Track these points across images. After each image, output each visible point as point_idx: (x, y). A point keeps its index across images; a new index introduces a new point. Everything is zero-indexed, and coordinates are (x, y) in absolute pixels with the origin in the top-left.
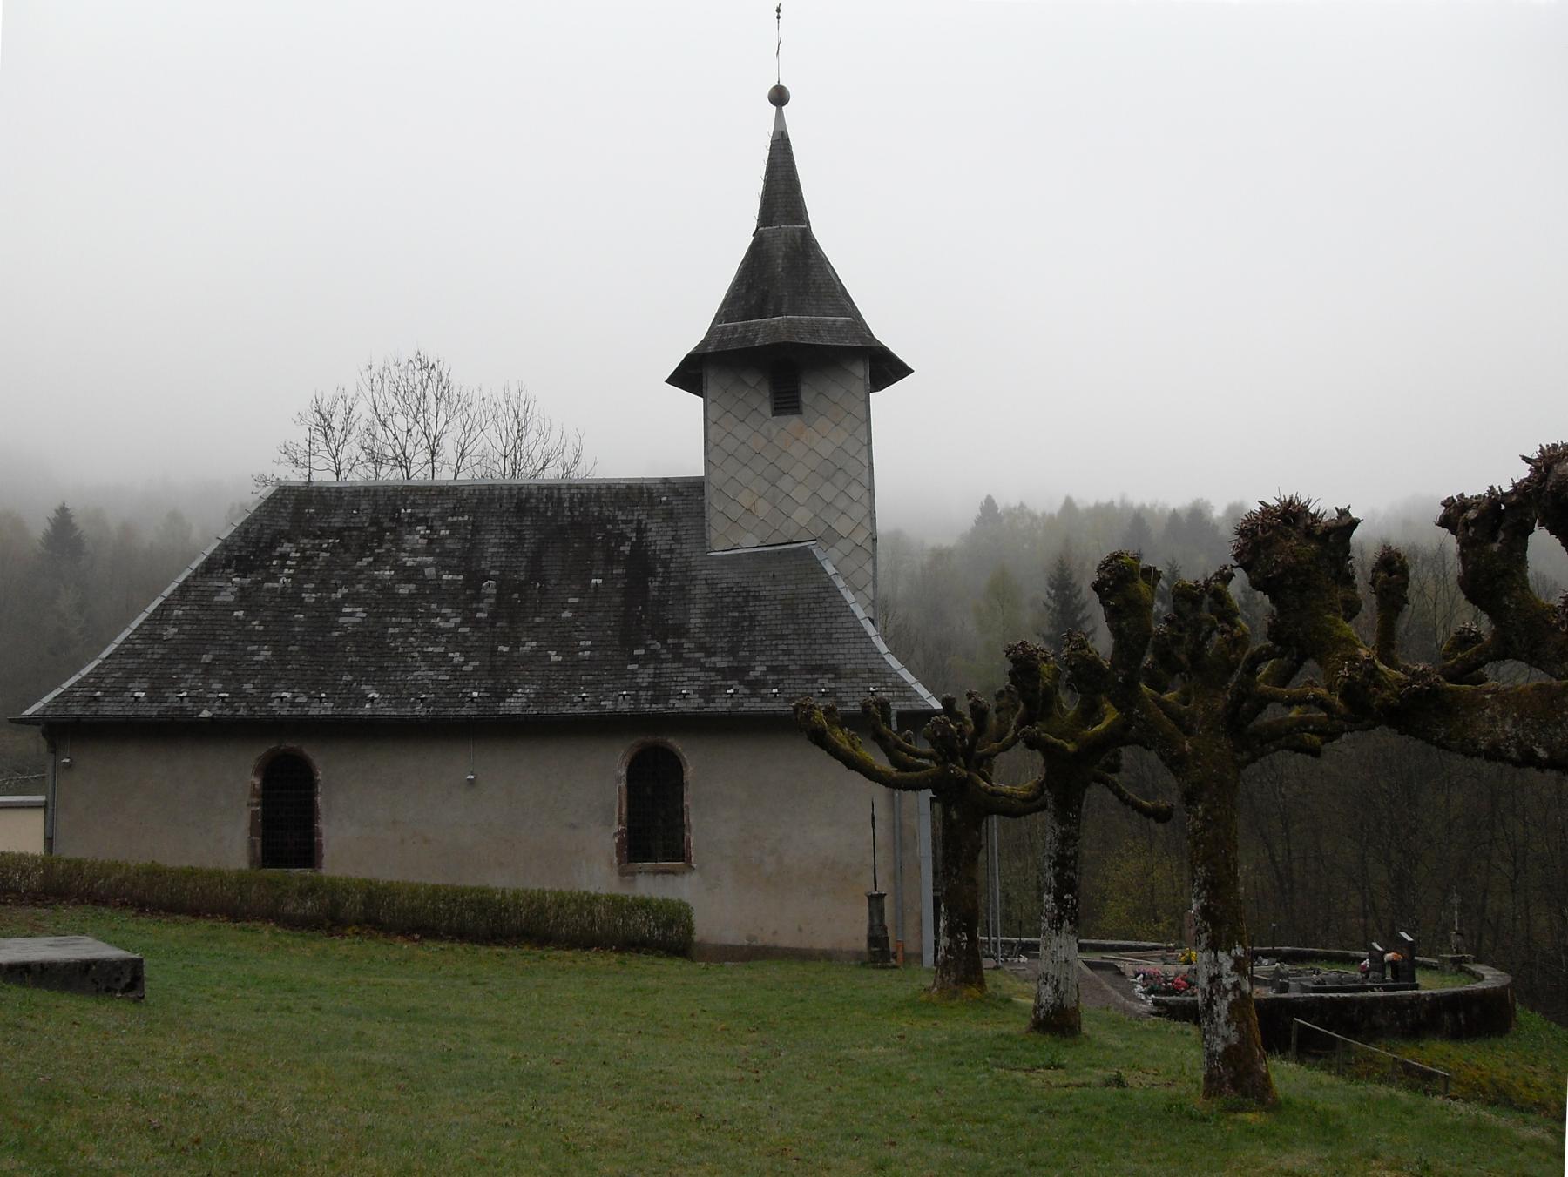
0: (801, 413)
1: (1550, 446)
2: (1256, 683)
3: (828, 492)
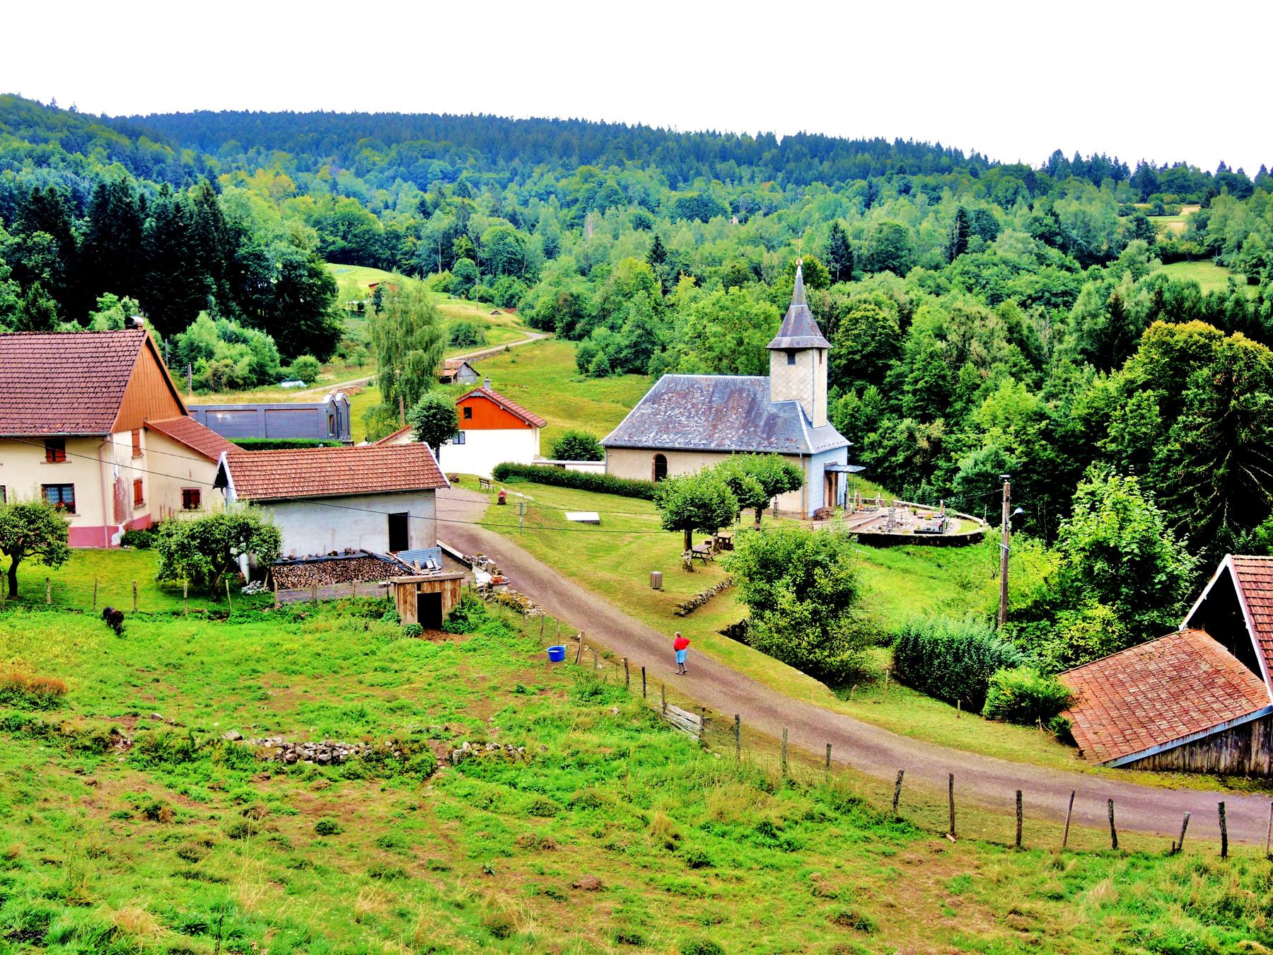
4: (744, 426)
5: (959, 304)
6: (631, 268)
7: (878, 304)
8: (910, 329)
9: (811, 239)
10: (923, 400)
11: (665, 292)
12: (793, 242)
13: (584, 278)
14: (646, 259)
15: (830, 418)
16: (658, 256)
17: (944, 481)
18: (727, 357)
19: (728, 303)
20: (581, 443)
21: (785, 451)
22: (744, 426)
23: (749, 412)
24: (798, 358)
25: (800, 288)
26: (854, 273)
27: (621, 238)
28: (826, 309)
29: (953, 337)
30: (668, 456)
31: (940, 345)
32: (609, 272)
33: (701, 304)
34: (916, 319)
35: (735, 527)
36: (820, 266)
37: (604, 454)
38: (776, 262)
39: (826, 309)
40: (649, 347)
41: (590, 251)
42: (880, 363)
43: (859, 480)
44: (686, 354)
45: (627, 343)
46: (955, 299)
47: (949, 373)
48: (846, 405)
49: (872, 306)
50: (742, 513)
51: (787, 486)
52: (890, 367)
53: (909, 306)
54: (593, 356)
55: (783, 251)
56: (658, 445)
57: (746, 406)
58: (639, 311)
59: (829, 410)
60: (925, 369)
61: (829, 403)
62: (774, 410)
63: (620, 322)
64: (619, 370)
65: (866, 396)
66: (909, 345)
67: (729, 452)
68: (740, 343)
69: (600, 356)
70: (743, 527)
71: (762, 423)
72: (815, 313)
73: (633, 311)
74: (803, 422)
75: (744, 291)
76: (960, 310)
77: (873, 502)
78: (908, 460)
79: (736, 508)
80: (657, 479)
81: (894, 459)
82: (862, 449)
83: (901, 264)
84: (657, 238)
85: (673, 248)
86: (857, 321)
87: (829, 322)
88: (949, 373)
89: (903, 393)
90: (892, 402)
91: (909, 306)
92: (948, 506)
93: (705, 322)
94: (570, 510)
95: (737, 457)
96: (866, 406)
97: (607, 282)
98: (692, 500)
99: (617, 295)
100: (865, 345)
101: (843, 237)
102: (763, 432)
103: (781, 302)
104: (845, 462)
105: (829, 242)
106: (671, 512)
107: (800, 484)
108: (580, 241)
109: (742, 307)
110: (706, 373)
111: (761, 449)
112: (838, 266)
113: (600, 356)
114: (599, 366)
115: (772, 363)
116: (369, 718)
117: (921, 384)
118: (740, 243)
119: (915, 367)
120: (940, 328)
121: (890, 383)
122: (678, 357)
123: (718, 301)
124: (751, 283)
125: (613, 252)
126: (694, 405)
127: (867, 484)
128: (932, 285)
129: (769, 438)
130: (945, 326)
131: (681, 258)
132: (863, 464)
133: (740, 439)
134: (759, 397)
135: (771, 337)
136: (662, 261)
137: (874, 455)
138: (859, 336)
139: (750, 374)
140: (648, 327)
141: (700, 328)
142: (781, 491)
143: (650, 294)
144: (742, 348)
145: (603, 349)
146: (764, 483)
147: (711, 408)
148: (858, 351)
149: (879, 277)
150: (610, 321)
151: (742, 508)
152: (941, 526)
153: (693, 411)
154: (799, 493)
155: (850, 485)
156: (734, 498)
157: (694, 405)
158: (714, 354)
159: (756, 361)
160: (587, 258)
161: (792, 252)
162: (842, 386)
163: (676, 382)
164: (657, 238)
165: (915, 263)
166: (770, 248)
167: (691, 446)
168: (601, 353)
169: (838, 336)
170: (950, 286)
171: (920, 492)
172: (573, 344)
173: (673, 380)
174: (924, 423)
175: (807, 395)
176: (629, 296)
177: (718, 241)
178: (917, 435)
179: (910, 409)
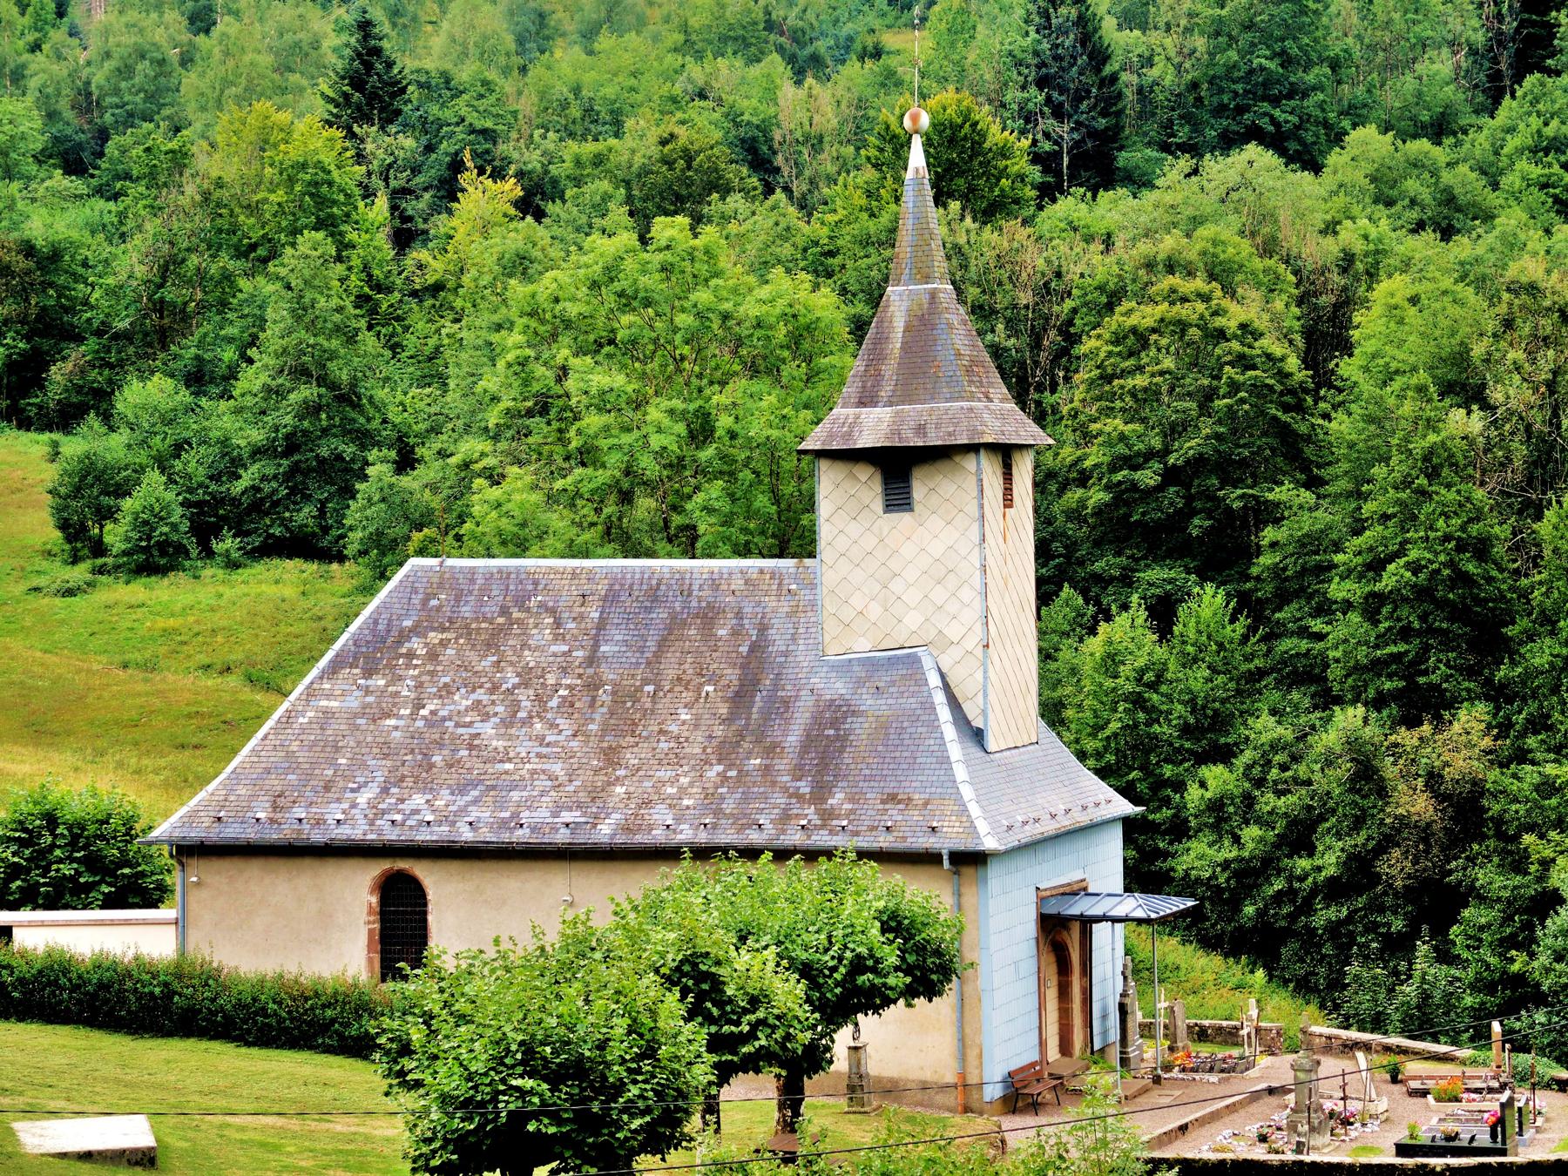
0: (912, 510)
1: (459, 195)
2: (1258, 546)
3: (939, 595)
4: (726, 752)
5: (1528, 267)
6: (264, 144)
7: (1221, 273)
8: (1348, 368)
9: (961, 30)
10: (1405, 633)
11: (404, 237)
12: (890, 40)
13: (77, 185)
14: (322, 109)
15: (1052, 713)
16: (372, 97)
17: (1506, 944)
18: (651, 486)
19: (651, 282)
20: (77, 831)
21: (884, 842)
22: (726, 752)
23: (741, 698)
24: (921, 486)
25: (921, 219)
26: (1124, 159)
27: (225, 25)
28: (1025, 298)
29: (1509, 393)
30: (429, 876)
31: (1465, 423)
32: (180, 159)
33: (546, 284)
34: (1368, 326)
35: (701, 1154)
36: (996, 135)
37: (174, 879)
38: (828, 119)
39: (1025, 298)
40: (349, 450)
41: (99, 79)
42: (1234, 497)
43: (1172, 950)
44: (495, 479)
45: (257, 436)
46: (1513, 246)
47: (1502, 531)
48: (1111, 663)
49: (1199, 284)
50: (726, 1093)
51: (897, 980)
52: (1270, 514)
53: (1337, 280)
54: (122, 491)
55: (855, 74)
56: (392, 835)
57: (732, 675)
58: (301, 311)
59: (1047, 680)
60: (1408, 518)
61: (1046, 656)
62: (839, 688)
63: (229, 354)
64: (227, 544)
65: (1187, 623)
66: (1342, 426)
67: (668, 854)
68: (701, 430)
69: (153, 489)
70: (730, 1149)
71: (793, 739)
72: (981, 312)
73: (278, 315)
74: (949, 731)
75: (709, 233)
76: (1532, 289)
77: (1230, 1036)
78: (1359, 872)
79: (702, 1074)
80: (388, 971)
81: (1303, 864)
82: (1180, 830)
83: (1305, 119)
84: (365, 26)
85: (430, 64)
86: (1139, 340)
87: (1036, 345)
88: (1502, 531)
89: (1324, 609)
90: (1287, 645)
91: (1337, 280)
92: (1519, 1045)
93: (563, 352)
94: (30, 1112)
95: (700, 872)
96: (1190, 662)
97: (170, 197)
98: (528, 1048)
99: (214, 248)
100: (1175, 430)
101: (1082, 21)
102: (798, 772)
103: (855, 269)
104: (1117, 882)
105: (1026, 41)
106: (445, 1099)
107: (946, 971)
108: (57, 36)
109: (702, 296)
110: (573, 551)
111: (794, 838)
112: (1064, 130)
113: (153, 489)
114: (144, 526)
115: (824, 507)
116: (613, 907)
117: (1393, 576)
118: (689, 46)
119: (1369, 508)
120: (1461, 358)
121: (1277, 572)
122: (463, 488)
123: (611, 272)
124: (735, 201)
125: (190, 81)
126: (527, 677)
127: (1204, 965)
128: (1425, 195)
129: (820, 794)
130: (1478, 350)
131: (461, 105)
132: (1186, 886)
133: (711, 802)
134: (778, 638)
135: (819, 408)
136: (389, 116)
137: (1229, 852)
138: (1149, 396)
139: (744, 551)
140: (341, 374)
141: (543, 375)
142: (876, 1000)
143: (344, 246)
144: (707, 453)
145: (162, 464)
146: (806, 971)
147: (593, 686)
148: (1150, 455)
149: (1222, 169)
150: (187, 351)
151: (725, 1073)
152: (1500, 1123)
153: (525, 698)
154: (943, 1005)
155: (1139, 971)
156: (695, 1035)
157: (527, 677)
158: (602, 477)
159: (762, 501)
160: (86, 102)
161: (891, 81)
162: (1092, 587)
163: (457, 587)
164: (365, 26)
165: (1357, 114)
166: (805, 66)
167: (521, 836)
168: (154, 477)
169: (1072, 396)
170: (1493, 199)
171: (1409, 990)
172: (34, 444)
173: (446, 581)
174: (1412, 722)
175: (962, 627)
176: (260, 254)
177: (604, 42)
178: (1389, 769)
179: (1357, 669)
